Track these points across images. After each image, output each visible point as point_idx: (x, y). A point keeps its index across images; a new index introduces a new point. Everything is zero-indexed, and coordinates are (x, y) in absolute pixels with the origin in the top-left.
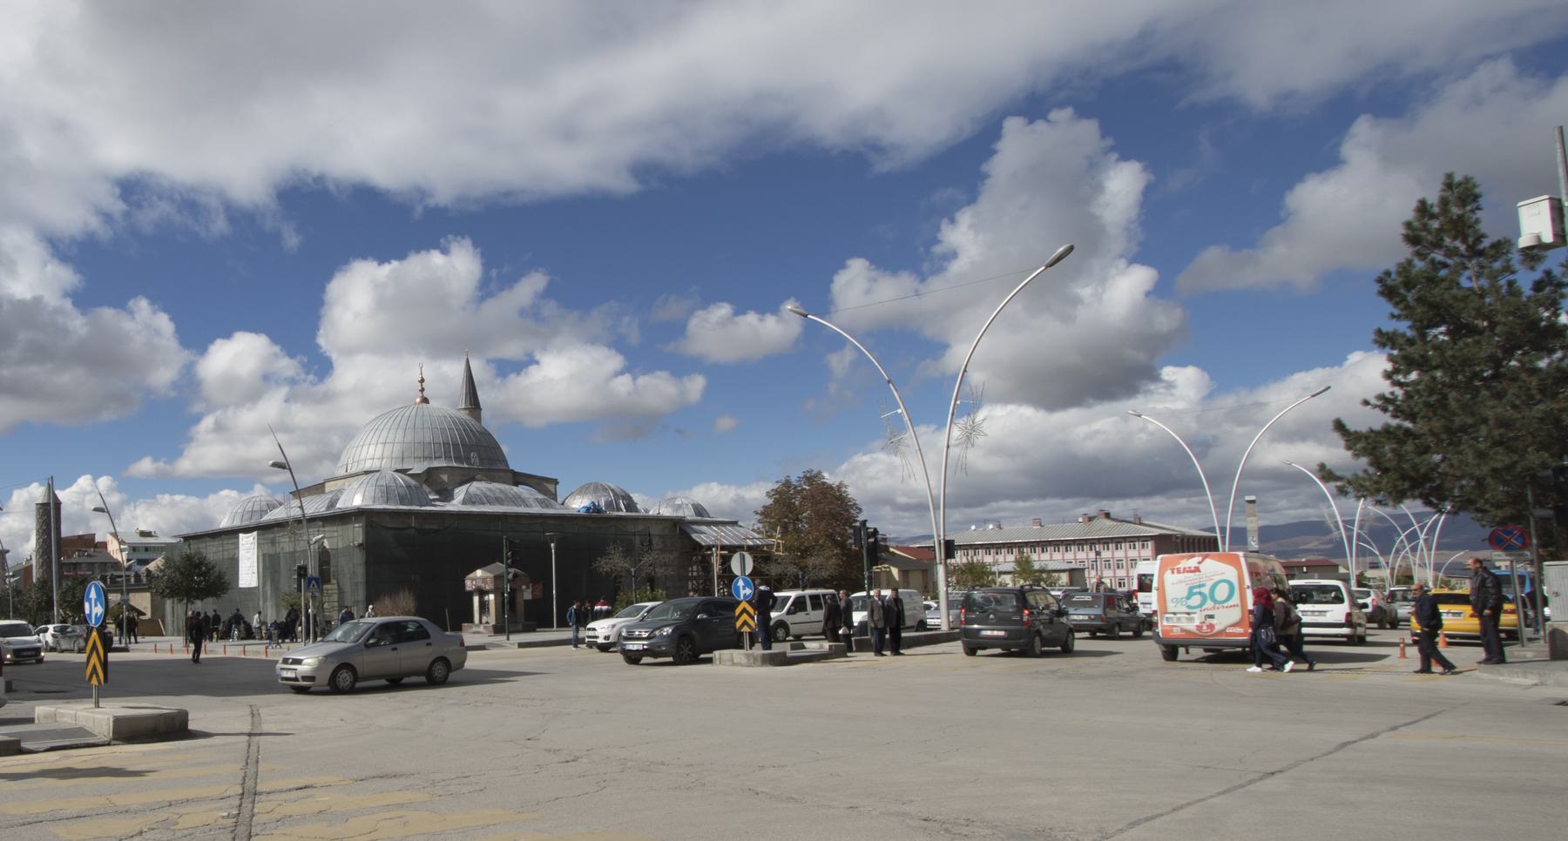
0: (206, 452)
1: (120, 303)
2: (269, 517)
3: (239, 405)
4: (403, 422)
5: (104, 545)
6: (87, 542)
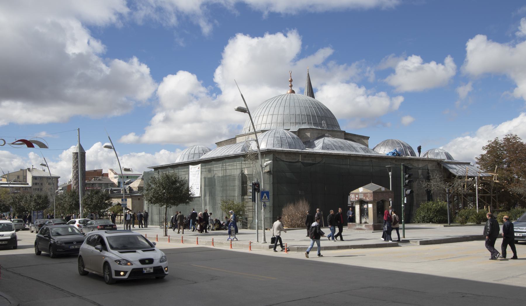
0: (158, 131)
1: (126, 58)
2: (204, 157)
3: (175, 110)
4: (283, 103)
5: (107, 175)
6: (98, 173)
